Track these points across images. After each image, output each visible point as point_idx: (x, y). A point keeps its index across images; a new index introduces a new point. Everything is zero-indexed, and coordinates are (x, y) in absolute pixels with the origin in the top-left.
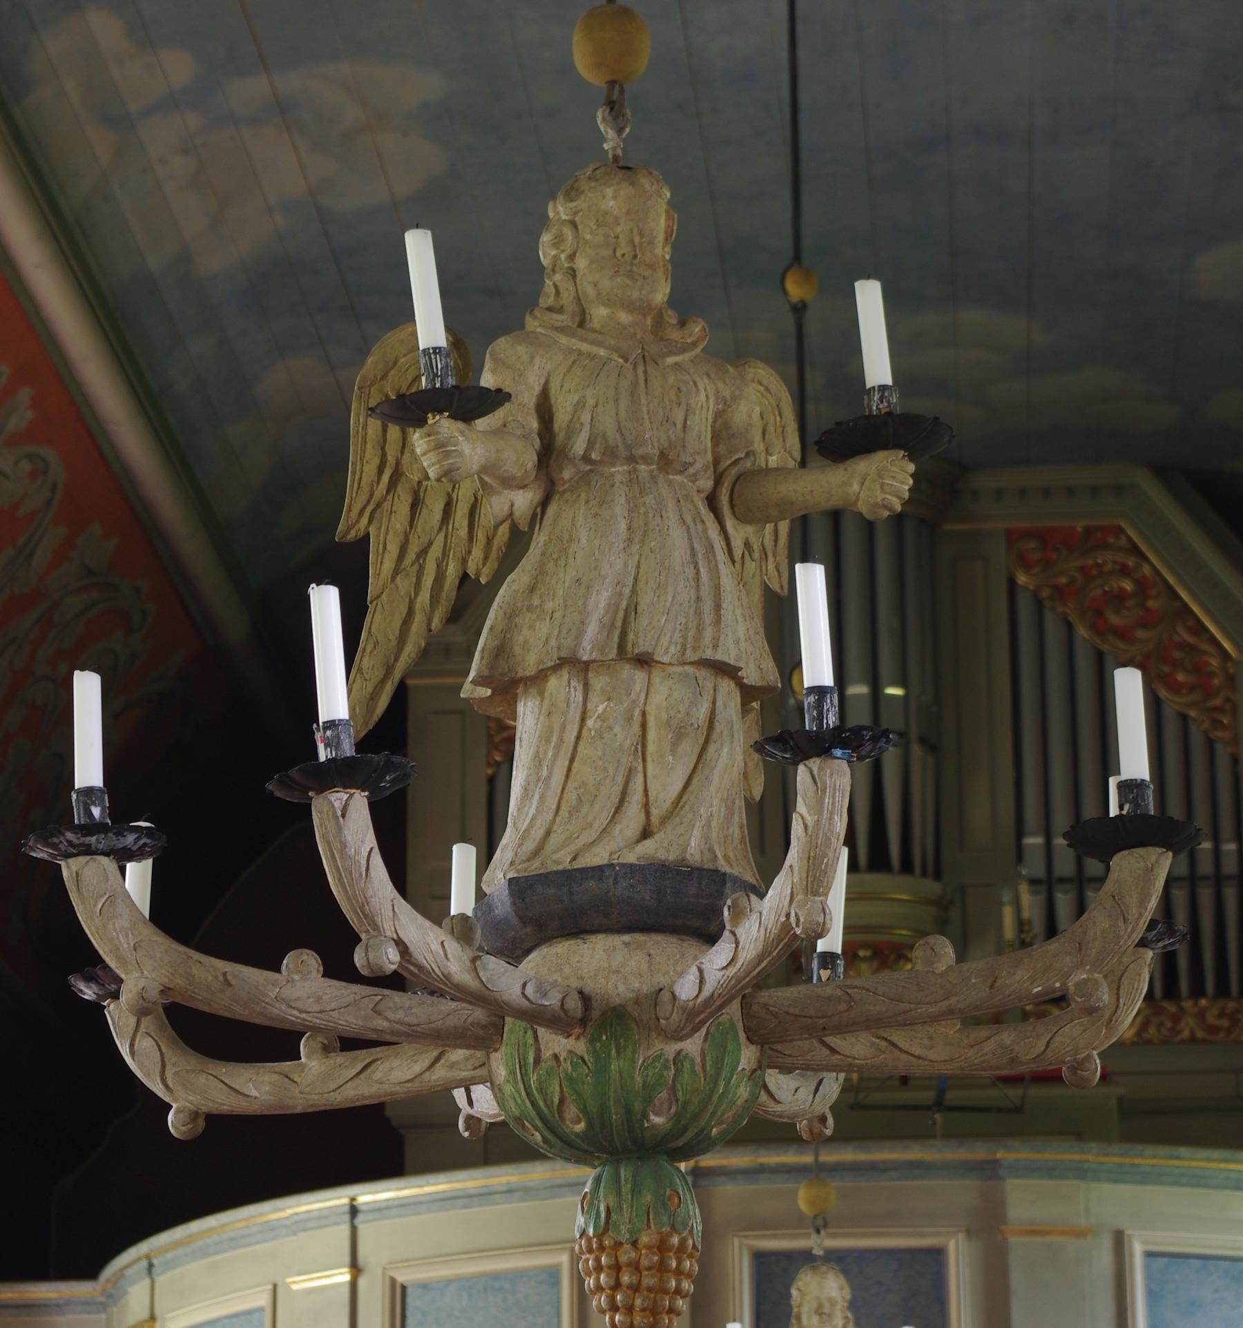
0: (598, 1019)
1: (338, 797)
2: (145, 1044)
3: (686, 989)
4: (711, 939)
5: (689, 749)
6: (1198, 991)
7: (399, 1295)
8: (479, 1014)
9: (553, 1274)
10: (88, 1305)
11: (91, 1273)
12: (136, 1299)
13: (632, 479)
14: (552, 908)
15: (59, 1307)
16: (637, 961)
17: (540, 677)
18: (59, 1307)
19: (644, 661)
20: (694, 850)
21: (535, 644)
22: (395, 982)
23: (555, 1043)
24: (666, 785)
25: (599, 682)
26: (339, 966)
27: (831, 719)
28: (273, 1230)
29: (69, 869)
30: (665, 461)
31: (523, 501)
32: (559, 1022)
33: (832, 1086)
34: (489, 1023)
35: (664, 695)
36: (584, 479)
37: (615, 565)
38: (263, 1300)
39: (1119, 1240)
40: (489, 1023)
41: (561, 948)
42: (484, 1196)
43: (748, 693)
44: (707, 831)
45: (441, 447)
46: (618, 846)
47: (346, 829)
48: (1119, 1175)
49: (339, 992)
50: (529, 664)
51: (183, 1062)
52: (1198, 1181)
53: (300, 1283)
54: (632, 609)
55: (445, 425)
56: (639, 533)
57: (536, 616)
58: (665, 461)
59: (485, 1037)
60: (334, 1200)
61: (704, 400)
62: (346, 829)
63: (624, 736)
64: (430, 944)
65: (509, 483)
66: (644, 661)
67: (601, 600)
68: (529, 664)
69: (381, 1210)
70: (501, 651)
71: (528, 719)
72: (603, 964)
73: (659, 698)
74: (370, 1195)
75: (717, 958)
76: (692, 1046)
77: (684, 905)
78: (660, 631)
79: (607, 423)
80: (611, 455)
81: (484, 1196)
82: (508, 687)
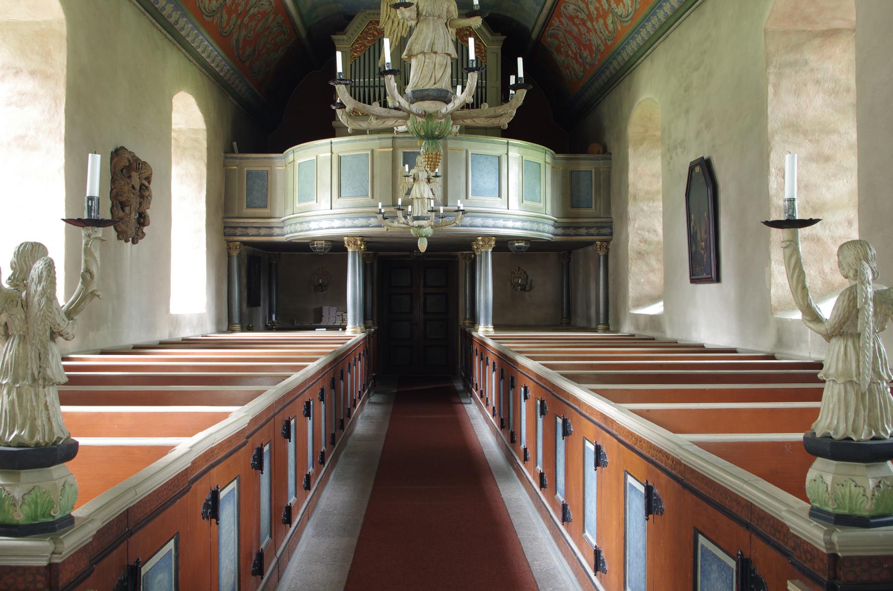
0: (427, 116)
1: (389, 76)
2: (344, 117)
3: (444, 111)
4: (447, 103)
5: (443, 69)
6: (375, 100)
7: (340, 158)
8: (406, 114)
9: (367, 155)
10: (281, 158)
11: (282, 153)
12: (291, 158)
13: (433, 20)
14: (420, 96)
15: (276, 158)
16: (434, 106)
17: (417, 55)
18: (276, 158)
19: (435, 53)
20: (444, 87)
21: (416, 49)
22: (396, 109)
23: (419, 119)
24: (439, 75)
25: (427, 56)
26: (385, 105)
27: (474, 65)
28: (316, 146)
29: (337, 87)
30: (439, 17)
31: (413, 23)
32: (420, 116)
33: (459, 127)
34: (408, 115)
35: (439, 59)
36: (425, 19)
37: (431, 35)
38: (315, 158)
39: (467, 151)
40: (408, 115)
41: (420, 103)
42: (355, 141)
43: (452, 59)
44: (445, 83)
45: (402, 13)
46: (430, 86)
47: (391, 82)
48: (467, 140)
49: (382, 110)
50: (415, 52)
51: (350, 121)
52: (481, 141)
53: (321, 155)
54: (434, 43)
55: (402, 9)
56: (435, 30)
57: (416, 44)
58: (439, 17)
59: (406, 118)
60: (328, 141)
61: (445, 6)
62: (391, 82)
63: (432, 66)
64: (404, 103)
65: (412, 19)
66: (435, 53)
67: (428, 42)
68: (415, 52)
69: (336, 143)
70: (410, 50)
71: (414, 62)
72: (428, 106)
73: (438, 59)
74: (334, 140)
75: (450, 107)
76: (443, 121)
77: (444, 97)
78: (438, 47)
79: (429, 9)
80: (430, 15)
81: (355, 141)
82: (410, 56)
